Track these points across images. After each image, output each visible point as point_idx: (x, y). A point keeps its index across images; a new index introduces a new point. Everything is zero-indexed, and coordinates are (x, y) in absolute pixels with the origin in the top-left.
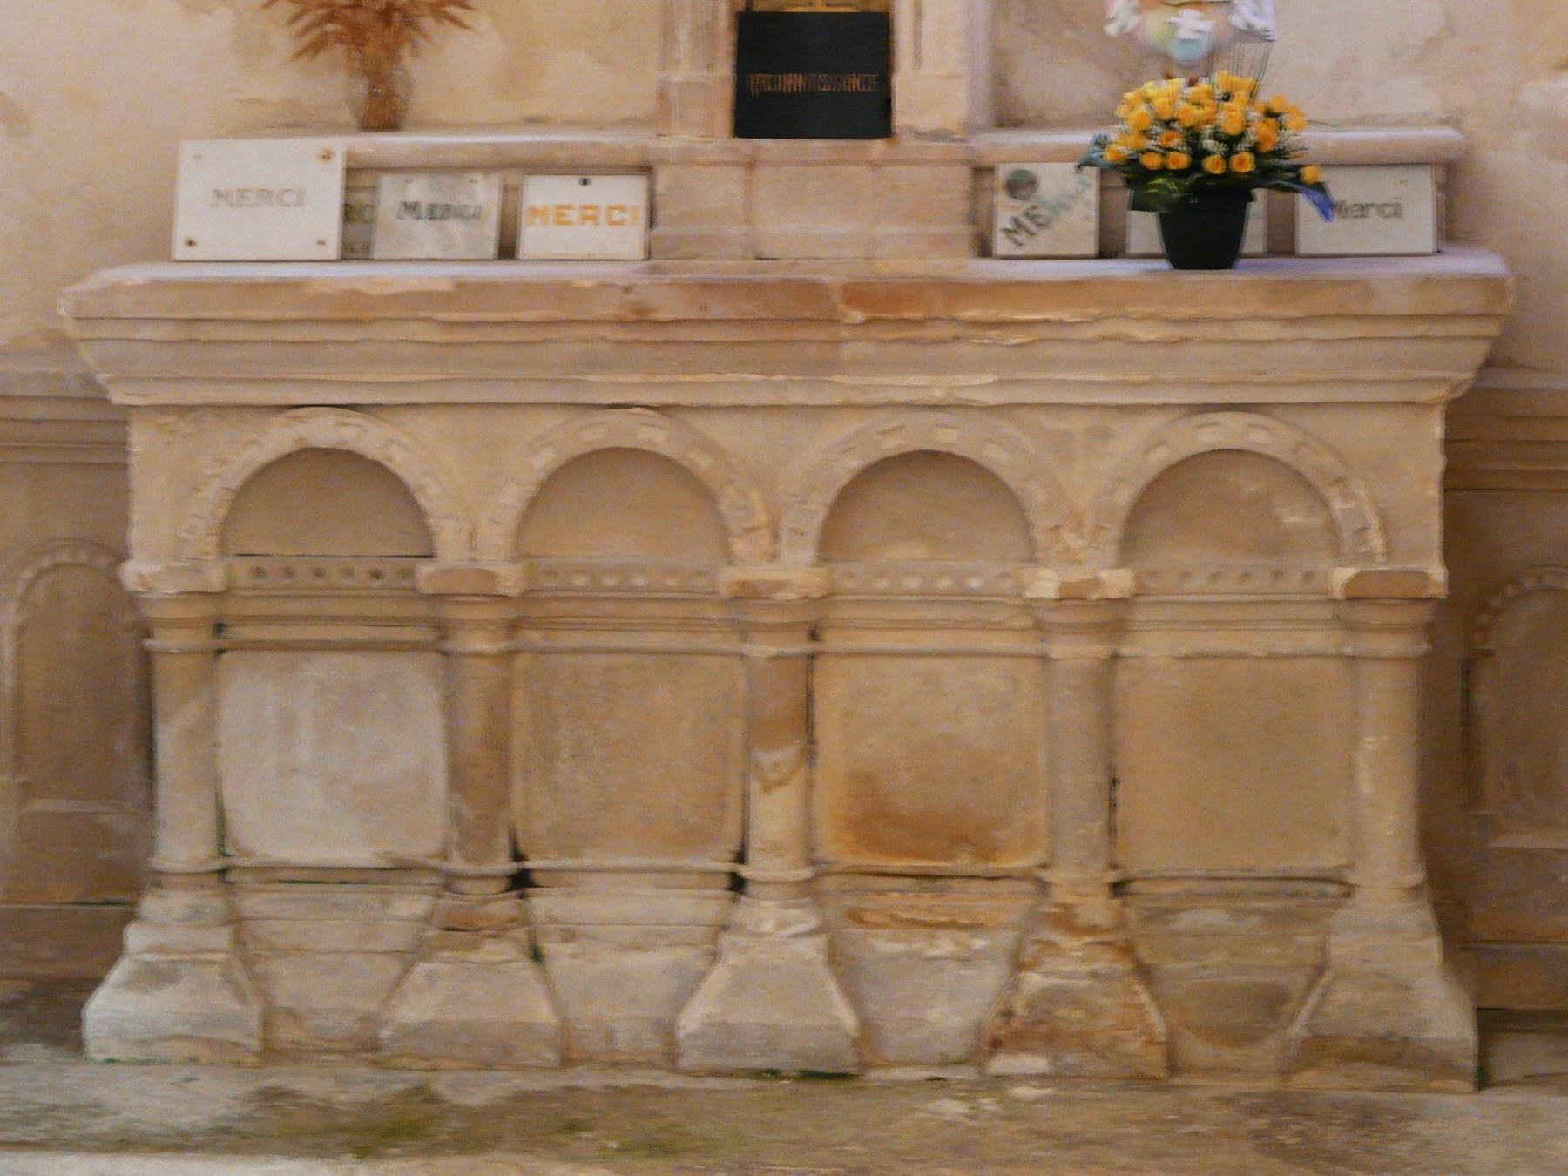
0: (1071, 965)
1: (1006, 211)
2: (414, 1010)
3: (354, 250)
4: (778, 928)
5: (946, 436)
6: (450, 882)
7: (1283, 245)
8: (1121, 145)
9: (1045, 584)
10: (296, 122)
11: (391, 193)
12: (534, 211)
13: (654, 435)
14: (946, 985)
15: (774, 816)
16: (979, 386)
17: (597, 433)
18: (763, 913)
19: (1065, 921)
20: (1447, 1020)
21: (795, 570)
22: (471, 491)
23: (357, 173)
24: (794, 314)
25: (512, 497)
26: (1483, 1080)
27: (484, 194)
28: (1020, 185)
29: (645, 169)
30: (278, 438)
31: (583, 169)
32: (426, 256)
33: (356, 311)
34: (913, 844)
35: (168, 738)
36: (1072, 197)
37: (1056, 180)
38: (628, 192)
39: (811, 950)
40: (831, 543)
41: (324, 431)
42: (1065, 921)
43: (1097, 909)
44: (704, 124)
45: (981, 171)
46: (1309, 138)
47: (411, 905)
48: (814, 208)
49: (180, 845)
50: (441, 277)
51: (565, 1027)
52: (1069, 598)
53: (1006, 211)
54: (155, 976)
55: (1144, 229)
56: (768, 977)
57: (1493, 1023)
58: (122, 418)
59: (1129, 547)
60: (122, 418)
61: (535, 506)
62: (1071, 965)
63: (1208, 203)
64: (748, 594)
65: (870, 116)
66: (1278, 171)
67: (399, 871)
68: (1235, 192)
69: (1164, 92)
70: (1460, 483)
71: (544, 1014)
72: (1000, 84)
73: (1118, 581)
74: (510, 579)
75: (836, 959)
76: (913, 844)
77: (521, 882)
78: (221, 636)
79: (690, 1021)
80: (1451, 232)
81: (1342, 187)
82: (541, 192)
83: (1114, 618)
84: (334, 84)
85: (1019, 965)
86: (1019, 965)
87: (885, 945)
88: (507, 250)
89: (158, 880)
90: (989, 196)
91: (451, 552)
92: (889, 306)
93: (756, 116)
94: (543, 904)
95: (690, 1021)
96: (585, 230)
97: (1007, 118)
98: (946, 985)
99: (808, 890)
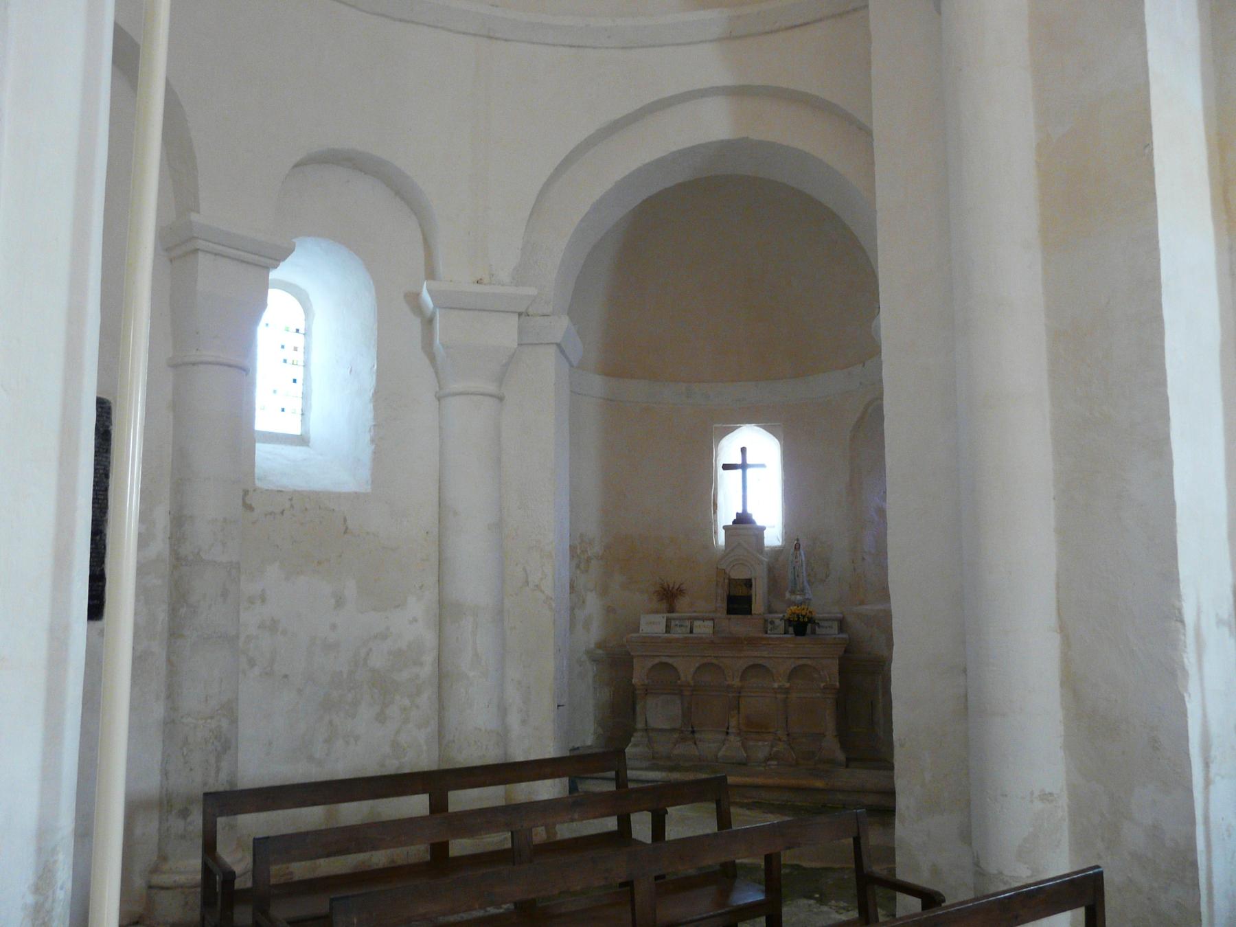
0: (781, 747)
1: (770, 626)
2: (676, 752)
3: (668, 631)
4: (734, 740)
5: (760, 662)
6: (682, 732)
7: (813, 632)
8: (787, 616)
9: (776, 685)
10: (656, 612)
11: (673, 623)
12: (184, 813)
13: (715, 661)
14: (761, 749)
15: (733, 722)
16: (765, 654)
17: (705, 660)
18: (732, 738)
19: (780, 740)
20: (840, 756)
21: (737, 682)
22: (686, 669)
23: (668, 620)
24: (736, 642)
25: (692, 670)
26: (847, 766)
27: (688, 623)
28: (772, 623)
29: (713, 619)
30: (657, 661)
31: (704, 619)
32: (678, 633)
33: (669, 641)
34: (755, 727)
35: (638, 708)
36: (781, 625)
37: (777, 622)
38: (710, 623)
39: (739, 744)
40: (743, 678)
41: (664, 660)
42: (780, 740)
43: (785, 738)
44: (722, 613)
45: (766, 621)
46: (817, 616)
47: (676, 735)
48: (739, 626)
49: (640, 725)
50: (681, 636)
51: (515, 904)
52: (780, 687)
53: (770, 626)
54: (635, 745)
55: (791, 630)
56: (732, 748)
57: (848, 760)
58: (632, 658)
59: (789, 679)
60: (632, 658)
61: (695, 673)
62: (781, 747)
63: (801, 625)
64: (729, 686)
65: (748, 611)
66: (811, 620)
67: (673, 730)
68: (804, 625)
69: (793, 608)
70: (842, 671)
71: (697, 753)
72: (770, 606)
73: (787, 685)
74: (692, 683)
75: (743, 745)
76: (755, 727)
77: (693, 732)
78: (647, 691)
79: (720, 754)
80: (841, 630)
81: (822, 624)
82: (697, 623)
83: (787, 691)
84: (664, 605)
85: (772, 747)
86: (772, 747)
87: (751, 743)
88: (691, 632)
89: (636, 730)
90: (767, 624)
91: (683, 679)
92: (752, 642)
93: (730, 611)
94: (697, 736)
95: (720, 754)
96: (703, 629)
97: (770, 612)
98: (761, 749)
99: (739, 734)
